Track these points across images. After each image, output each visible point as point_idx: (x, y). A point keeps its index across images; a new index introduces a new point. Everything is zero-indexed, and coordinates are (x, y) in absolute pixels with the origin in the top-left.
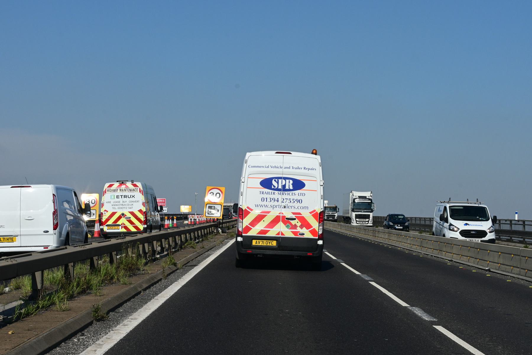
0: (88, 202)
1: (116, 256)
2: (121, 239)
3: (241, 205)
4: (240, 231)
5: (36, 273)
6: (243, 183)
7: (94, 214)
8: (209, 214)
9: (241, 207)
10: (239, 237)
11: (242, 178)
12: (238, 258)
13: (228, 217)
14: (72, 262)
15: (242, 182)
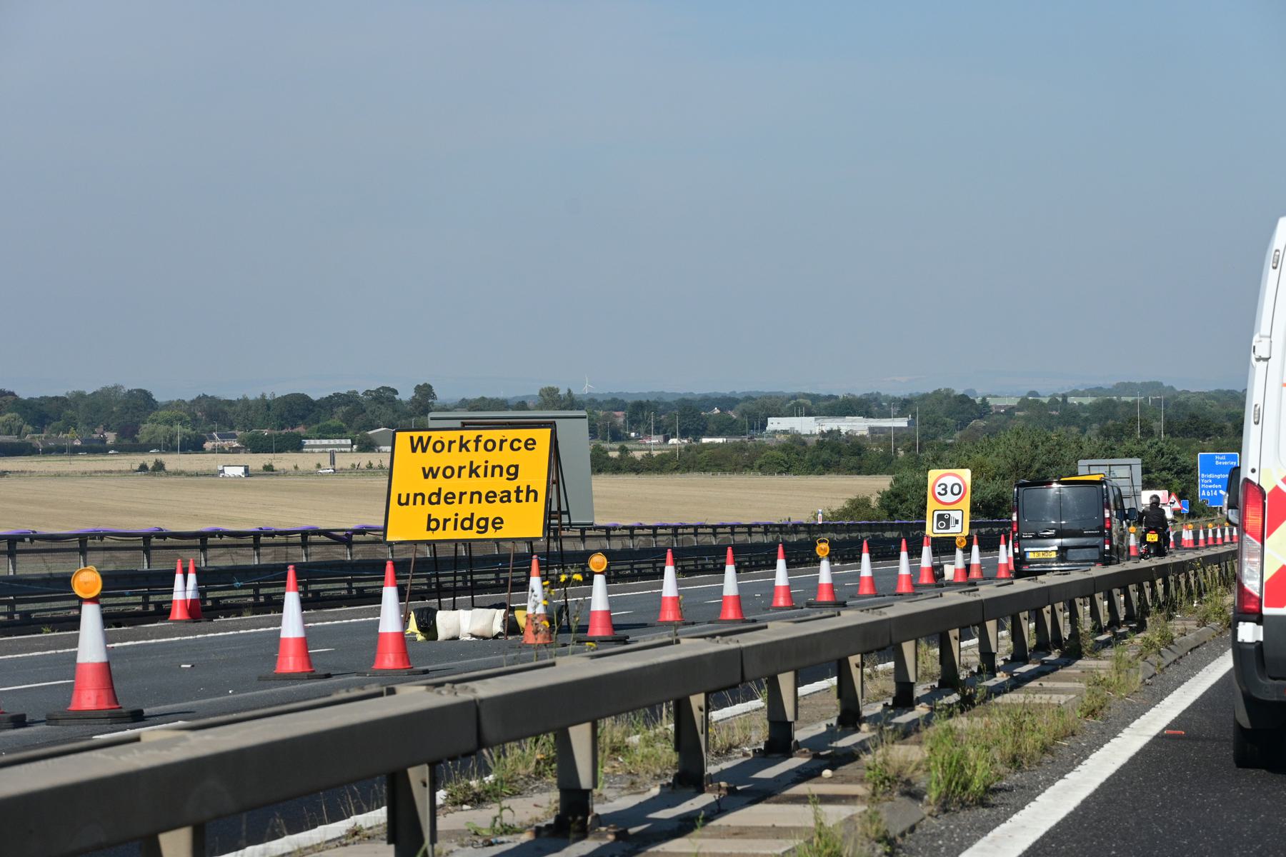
0: (943, 489)
1: (958, 642)
2: (967, 593)
3: (1253, 471)
4: (1251, 595)
5: (780, 677)
6: (1263, 364)
7: (957, 522)
8: (940, 529)
9: (1254, 478)
10: (1245, 621)
11: (1256, 338)
12: (1246, 723)
13: (1098, 540)
14: (955, 628)
15: (1258, 360)
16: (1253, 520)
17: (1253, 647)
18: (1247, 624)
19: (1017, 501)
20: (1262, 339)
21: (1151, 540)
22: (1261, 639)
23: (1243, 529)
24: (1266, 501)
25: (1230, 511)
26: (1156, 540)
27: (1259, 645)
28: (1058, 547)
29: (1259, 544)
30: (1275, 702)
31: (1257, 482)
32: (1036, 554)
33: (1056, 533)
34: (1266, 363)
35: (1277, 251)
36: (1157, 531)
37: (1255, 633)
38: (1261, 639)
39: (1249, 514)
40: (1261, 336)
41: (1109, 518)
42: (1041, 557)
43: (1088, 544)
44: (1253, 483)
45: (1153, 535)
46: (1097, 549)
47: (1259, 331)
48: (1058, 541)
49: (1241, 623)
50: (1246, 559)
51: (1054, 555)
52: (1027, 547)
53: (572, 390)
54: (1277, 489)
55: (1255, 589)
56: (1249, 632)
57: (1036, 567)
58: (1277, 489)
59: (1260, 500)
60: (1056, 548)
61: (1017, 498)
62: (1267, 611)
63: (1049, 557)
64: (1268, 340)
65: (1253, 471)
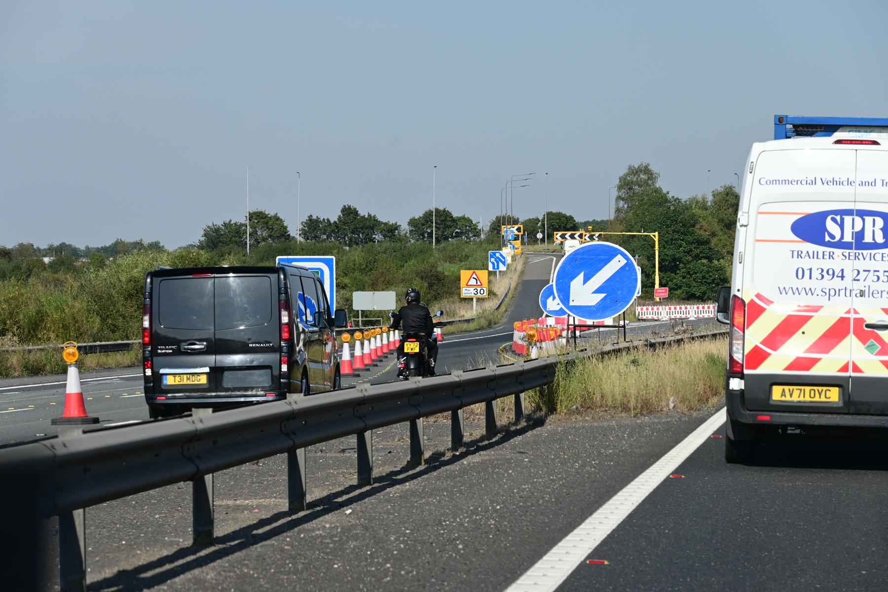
4: (738, 362)
6: (744, 229)
9: (739, 294)
13: (274, 357)
15: (741, 226)
16: (738, 319)
17: (739, 392)
18: (735, 379)
19: (151, 298)
20: (744, 214)
21: (409, 351)
22: (743, 388)
23: (732, 325)
24: (746, 309)
25: (719, 314)
26: (417, 350)
27: (742, 391)
28: (211, 368)
29: (742, 333)
30: (750, 424)
31: (740, 297)
32: (178, 378)
33: (207, 346)
34: (745, 228)
35: (752, 162)
36: (417, 338)
37: (739, 384)
38: (743, 388)
39: (736, 315)
40: (743, 212)
41: (287, 324)
42: (185, 382)
43: (255, 364)
44: (738, 298)
45: (412, 344)
46: (269, 371)
47: (742, 209)
48: (211, 359)
49: (731, 379)
50: (734, 342)
51: (203, 380)
52: (165, 367)
53: (823, 308)
54: (752, 301)
55: (740, 359)
56: (736, 384)
57: (179, 398)
58: (752, 301)
59: (743, 307)
60: (207, 370)
61: (151, 293)
62: (746, 372)
63: (196, 382)
64: (747, 215)
65: (739, 290)
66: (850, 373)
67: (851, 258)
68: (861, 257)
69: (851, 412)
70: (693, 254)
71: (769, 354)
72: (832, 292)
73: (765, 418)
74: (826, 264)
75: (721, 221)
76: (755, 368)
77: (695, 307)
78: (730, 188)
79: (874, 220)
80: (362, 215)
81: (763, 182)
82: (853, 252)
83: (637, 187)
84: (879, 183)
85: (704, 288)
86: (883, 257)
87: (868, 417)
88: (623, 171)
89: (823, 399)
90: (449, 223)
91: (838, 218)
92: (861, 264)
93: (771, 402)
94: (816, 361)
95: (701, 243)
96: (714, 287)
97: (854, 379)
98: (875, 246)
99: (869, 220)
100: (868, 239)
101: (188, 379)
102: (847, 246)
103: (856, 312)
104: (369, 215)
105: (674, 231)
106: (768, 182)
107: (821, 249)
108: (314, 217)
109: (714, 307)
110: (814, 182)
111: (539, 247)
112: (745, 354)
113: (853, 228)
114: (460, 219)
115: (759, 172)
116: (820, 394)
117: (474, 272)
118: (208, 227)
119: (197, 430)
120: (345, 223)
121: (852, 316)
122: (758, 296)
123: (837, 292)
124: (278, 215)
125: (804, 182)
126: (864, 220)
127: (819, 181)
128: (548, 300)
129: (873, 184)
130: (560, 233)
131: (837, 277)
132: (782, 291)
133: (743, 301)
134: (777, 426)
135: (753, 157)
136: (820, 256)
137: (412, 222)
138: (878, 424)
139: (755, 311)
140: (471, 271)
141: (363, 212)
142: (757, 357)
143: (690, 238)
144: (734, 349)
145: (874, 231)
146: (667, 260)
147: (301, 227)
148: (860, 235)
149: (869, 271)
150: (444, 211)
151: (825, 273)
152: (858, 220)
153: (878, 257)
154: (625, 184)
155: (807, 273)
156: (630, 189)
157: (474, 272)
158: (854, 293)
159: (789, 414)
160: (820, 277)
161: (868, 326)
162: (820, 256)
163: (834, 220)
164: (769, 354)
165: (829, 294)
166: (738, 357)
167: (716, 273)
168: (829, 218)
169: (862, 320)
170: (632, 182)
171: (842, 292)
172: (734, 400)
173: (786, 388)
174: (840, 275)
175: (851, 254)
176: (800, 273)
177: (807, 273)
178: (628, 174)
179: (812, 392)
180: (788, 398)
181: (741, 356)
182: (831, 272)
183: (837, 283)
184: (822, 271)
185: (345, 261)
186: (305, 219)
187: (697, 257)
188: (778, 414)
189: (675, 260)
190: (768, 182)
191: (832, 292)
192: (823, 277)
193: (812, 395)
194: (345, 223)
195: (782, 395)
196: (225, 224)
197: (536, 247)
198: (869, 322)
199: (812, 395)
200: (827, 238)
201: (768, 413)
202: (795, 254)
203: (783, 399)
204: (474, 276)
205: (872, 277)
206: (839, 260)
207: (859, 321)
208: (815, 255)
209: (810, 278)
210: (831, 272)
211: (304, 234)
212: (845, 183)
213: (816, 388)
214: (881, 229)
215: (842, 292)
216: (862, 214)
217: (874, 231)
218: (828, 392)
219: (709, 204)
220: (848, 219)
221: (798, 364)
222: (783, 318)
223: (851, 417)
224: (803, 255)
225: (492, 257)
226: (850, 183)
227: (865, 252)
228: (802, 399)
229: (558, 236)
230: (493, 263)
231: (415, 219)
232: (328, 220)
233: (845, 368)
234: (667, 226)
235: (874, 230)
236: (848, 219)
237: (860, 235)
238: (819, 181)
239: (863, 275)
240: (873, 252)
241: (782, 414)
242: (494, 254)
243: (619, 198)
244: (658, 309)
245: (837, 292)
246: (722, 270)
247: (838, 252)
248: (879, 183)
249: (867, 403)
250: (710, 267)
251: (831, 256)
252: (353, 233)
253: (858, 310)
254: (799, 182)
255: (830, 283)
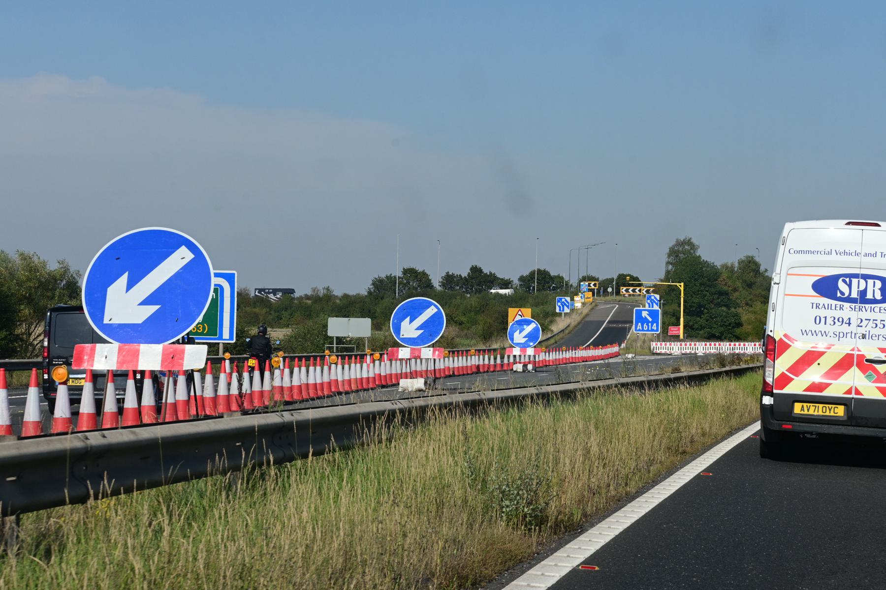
9: (771, 334)
15: (774, 284)
22: (772, 403)
29: (773, 363)
34: (777, 285)
38: (772, 403)
56: (767, 400)
63: (78, 384)
66: (853, 395)
67: (856, 310)
68: (863, 309)
69: (853, 424)
70: (716, 302)
71: (793, 379)
72: (841, 335)
73: (788, 426)
74: (838, 314)
75: (745, 281)
76: (782, 389)
77: (704, 343)
78: (752, 257)
79: (874, 282)
80: (485, 272)
81: (792, 251)
82: (858, 305)
83: (682, 255)
84: (879, 255)
85: (722, 329)
86: (880, 310)
87: (866, 429)
88: (672, 243)
89: (832, 414)
90: (548, 280)
91: (847, 280)
92: (864, 315)
93: (793, 415)
94: (828, 385)
95: (722, 293)
96: (729, 329)
97: (855, 399)
98: (874, 301)
99: (870, 282)
100: (869, 296)
101: (73, 382)
102: (854, 301)
103: (859, 351)
104: (491, 273)
105: (701, 284)
106: (796, 252)
107: (834, 302)
108: (451, 273)
109: (759, 345)
110: (830, 253)
111: (609, 298)
112: (775, 378)
113: (858, 288)
114: (555, 277)
115: (789, 245)
116: (830, 410)
117: (520, 310)
118: (376, 278)
119: (284, 423)
120: (472, 278)
121: (856, 353)
122: (786, 336)
123: (845, 335)
124: (425, 271)
125: (823, 253)
126: (867, 282)
127: (834, 252)
128: (403, 324)
129: (874, 255)
130: (625, 288)
131: (846, 323)
132: (804, 333)
133: (775, 340)
134: (799, 433)
135: (785, 233)
136: (833, 307)
137: (522, 279)
138: (873, 434)
139: (784, 347)
140: (518, 309)
141: (486, 271)
142: (784, 380)
143: (713, 290)
144: (767, 374)
145: (874, 290)
146: (694, 307)
147: (441, 280)
148: (863, 293)
149: (870, 320)
150: (545, 271)
151: (836, 321)
152: (862, 282)
153: (877, 310)
154: (673, 252)
155: (823, 320)
156: (677, 256)
157: (520, 310)
158: (857, 336)
159: (806, 424)
160: (832, 323)
161: (867, 361)
162: (833, 307)
163: (844, 281)
164: (793, 379)
165: (839, 336)
166: (769, 380)
167: (732, 318)
168: (841, 280)
169: (863, 356)
170: (679, 251)
171: (849, 335)
172: (766, 413)
173: (805, 405)
174: (848, 322)
175: (856, 307)
176: (817, 320)
177: (823, 320)
178: (676, 245)
179: (824, 408)
180: (806, 412)
181: (771, 380)
182: (841, 320)
183: (845, 328)
184: (835, 318)
185: (464, 305)
186: (444, 274)
187: (719, 305)
188: (798, 424)
189: (700, 306)
190: (796, 252)
191: (841, 335)
192: (835, 323)
193: (824, 411)
194: (472, 278)
195: (801, 410)
196: (387, 277)
197: (607, 298)
198: (868, 357)
199: (824, 411)
200: (839, 295)
201: (791, 423)
202: (815, 305)
203: (802, 412)
204: (520, 313)
205: (871, 324)
206: (847, 311)
207: (861, 357)
208: (829, 307)
209: (825, 324)
210: (841, 320)
211: (443, 285)
212: (853, 254)
213: (827, 406)
214: (879, 289)
215: (849, 335)
216: (866, 277)
217: (874, 290)
218: (836, 409)
219: (736, 269)
220: (855, 281)
221: (813, 387)
222: (804, 352)
223: (852, 428)
224: (820, 307)
225: (558, 301)
226: (857, 254)
227: (867, 306)
228: (816, 413)
229: (623, 290)
230: (560, 307)
231: (524, 277)
232: (460, 275)
233: (849, 392)
234: (696, 280)
235: (874, 290)
236: (855, 281)
237: (863, 293)
238: (834, 252)
239: (865, 323)
240: (873, 306)
241: (801, 424)
242: (561, 299)
243: (668, 263)
244: (695, 345)
245: (845, 335)
246: (737, 316)
247: (847, 305)
248: (879, 255)
249: (866, 418)
250: (727, 313)
251: (841, 308)
252: (478, 285)
253: (860, 349)
254: (819, 253)
255: (838, 328)
